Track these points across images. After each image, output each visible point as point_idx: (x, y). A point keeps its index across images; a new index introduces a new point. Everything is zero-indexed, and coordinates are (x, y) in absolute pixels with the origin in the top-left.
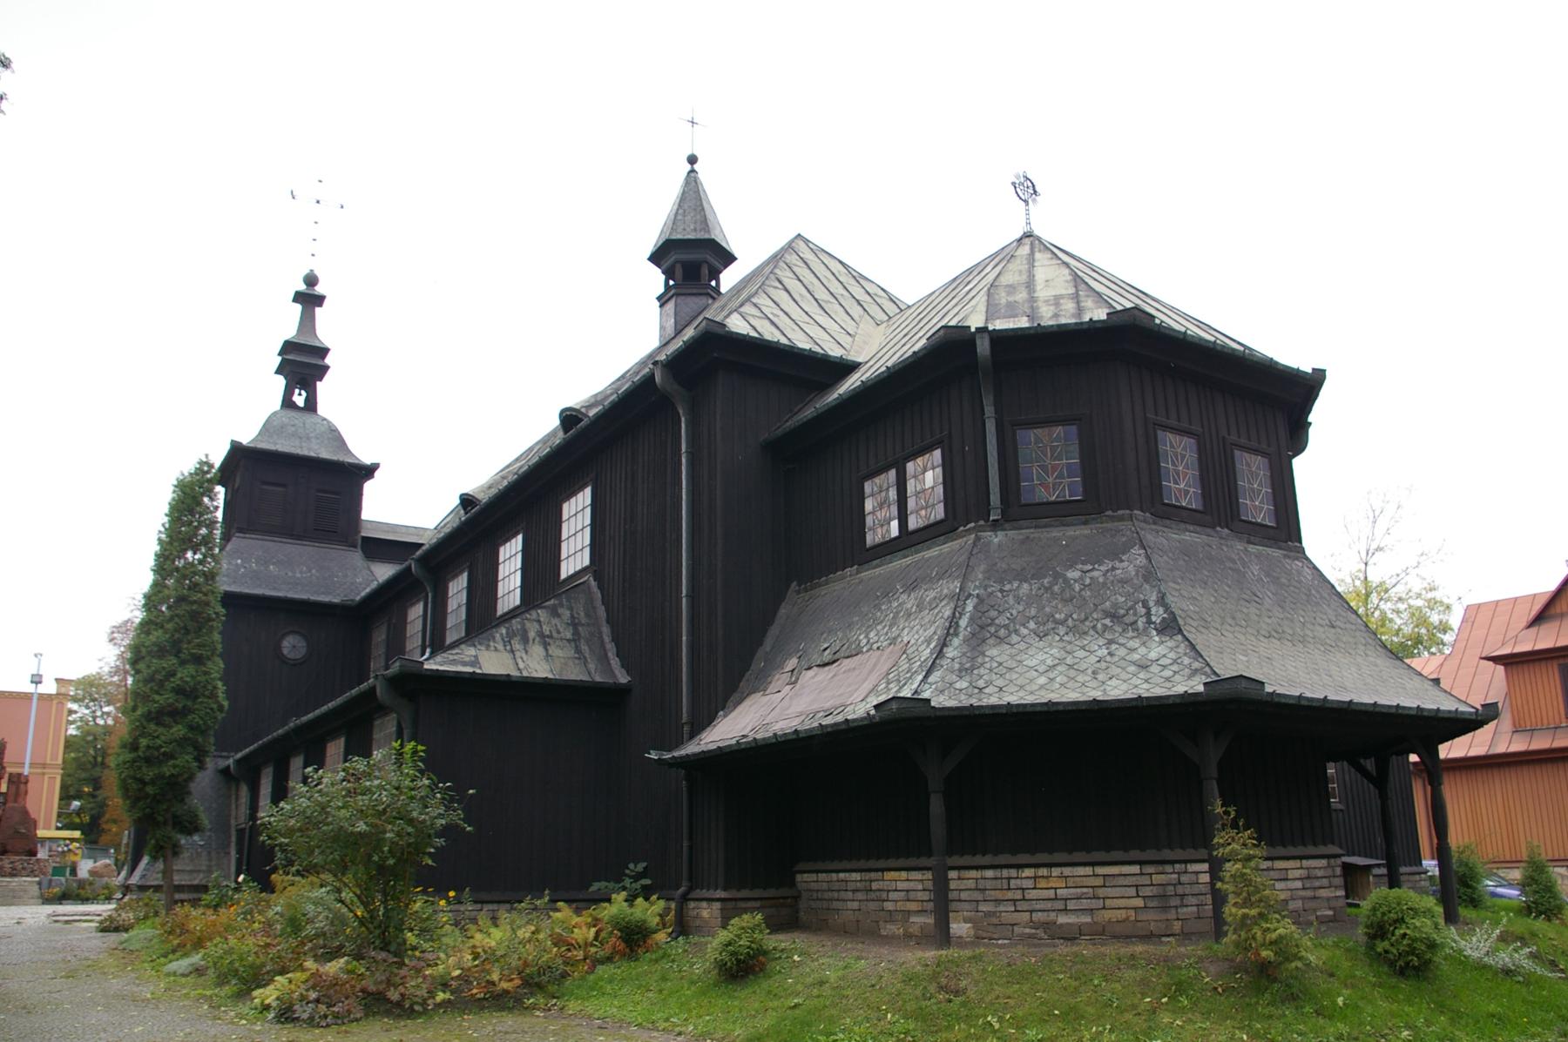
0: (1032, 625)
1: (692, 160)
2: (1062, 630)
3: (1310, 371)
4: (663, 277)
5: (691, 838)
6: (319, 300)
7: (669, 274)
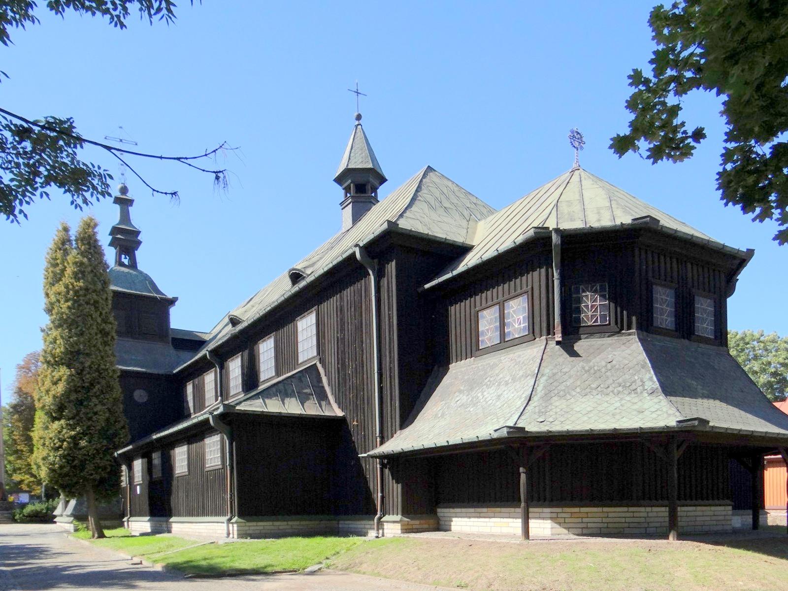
0: (578, 390)
1: (359, 117)
2: (595, 392)
3: (745, 250)
4: (343, 191)
5: (382, 491)
6: (130, 202)
7: (347, 190)
